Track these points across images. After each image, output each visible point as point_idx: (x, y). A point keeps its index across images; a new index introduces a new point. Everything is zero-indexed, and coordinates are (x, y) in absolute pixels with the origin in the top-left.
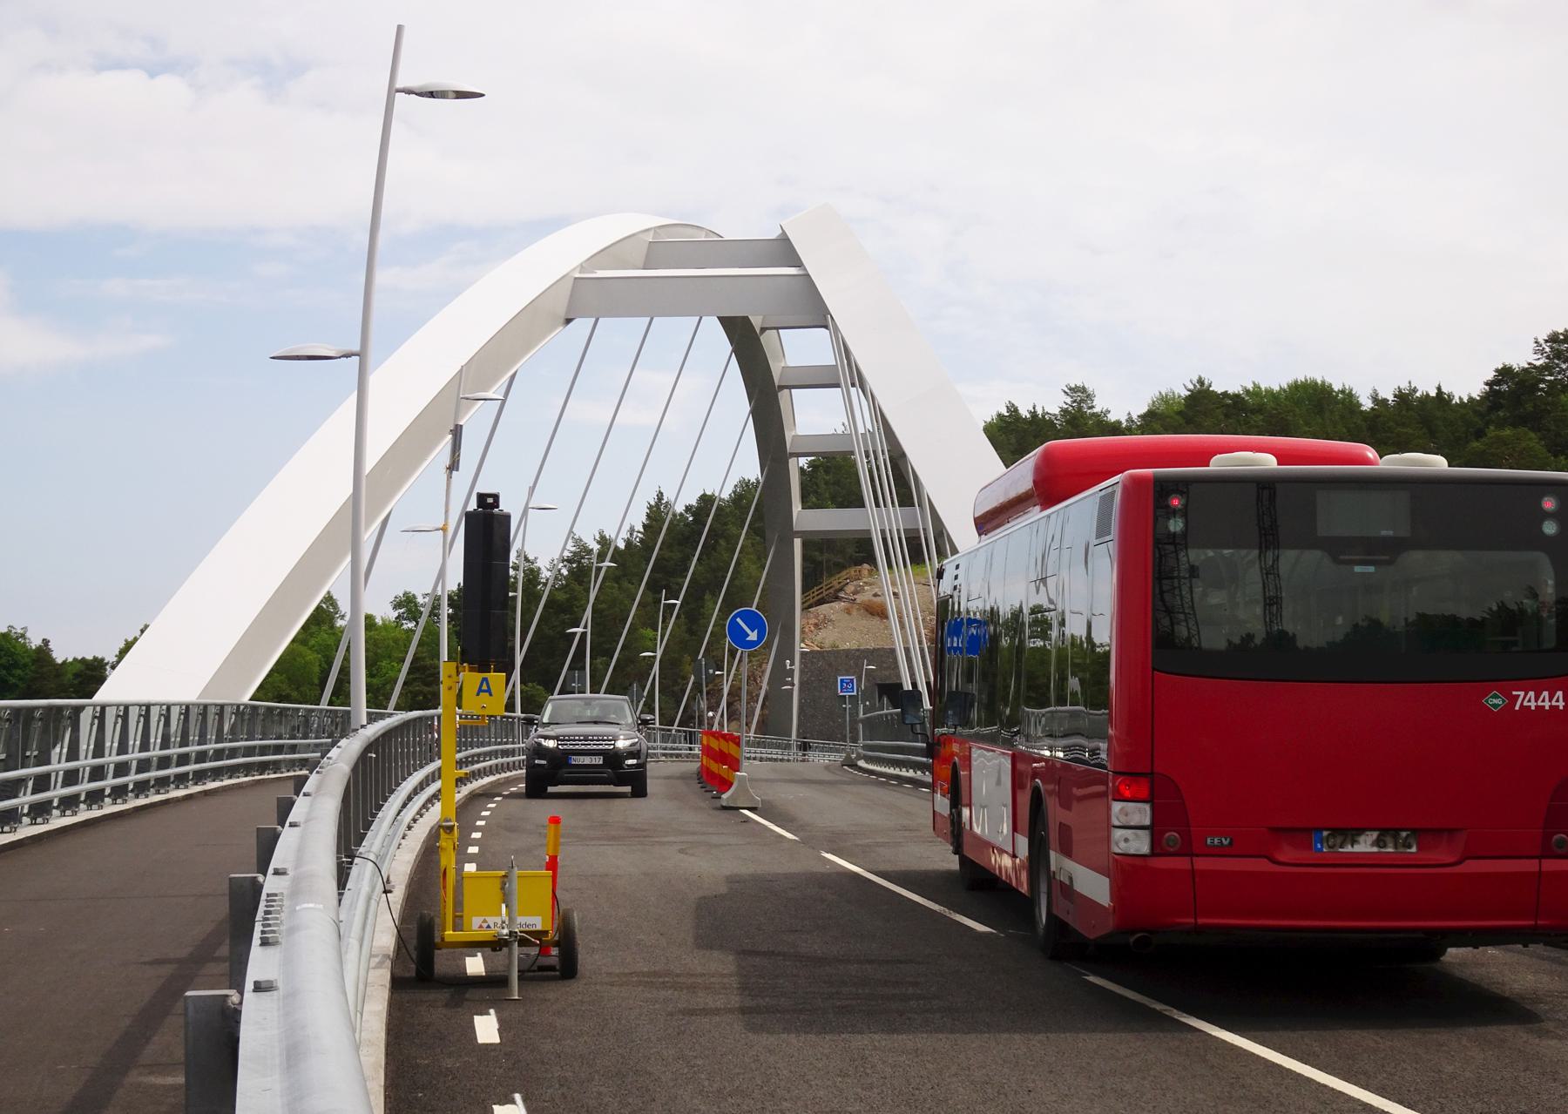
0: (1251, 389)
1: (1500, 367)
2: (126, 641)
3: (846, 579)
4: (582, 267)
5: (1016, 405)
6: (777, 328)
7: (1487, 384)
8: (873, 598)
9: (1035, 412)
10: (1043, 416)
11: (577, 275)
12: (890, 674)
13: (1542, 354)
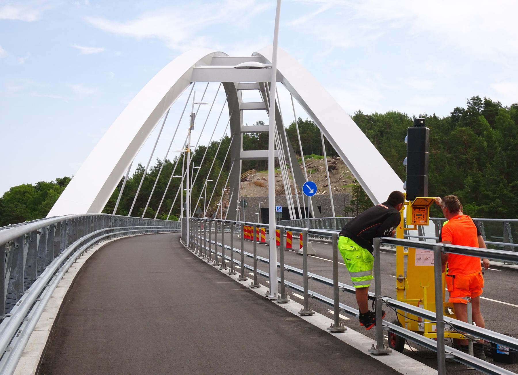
0: (375, 114)
1: (456, 108)
2: (5, 192)
3: (248, 174)
4: (196, 64)
5: (301, 118)
6: (241, 90)
7: (451, 113)
8: (257, 180)
9: (307, 121)
10: (310, 122)
11: (194, 67)
12: (265, 205)
13: (470, 104)
